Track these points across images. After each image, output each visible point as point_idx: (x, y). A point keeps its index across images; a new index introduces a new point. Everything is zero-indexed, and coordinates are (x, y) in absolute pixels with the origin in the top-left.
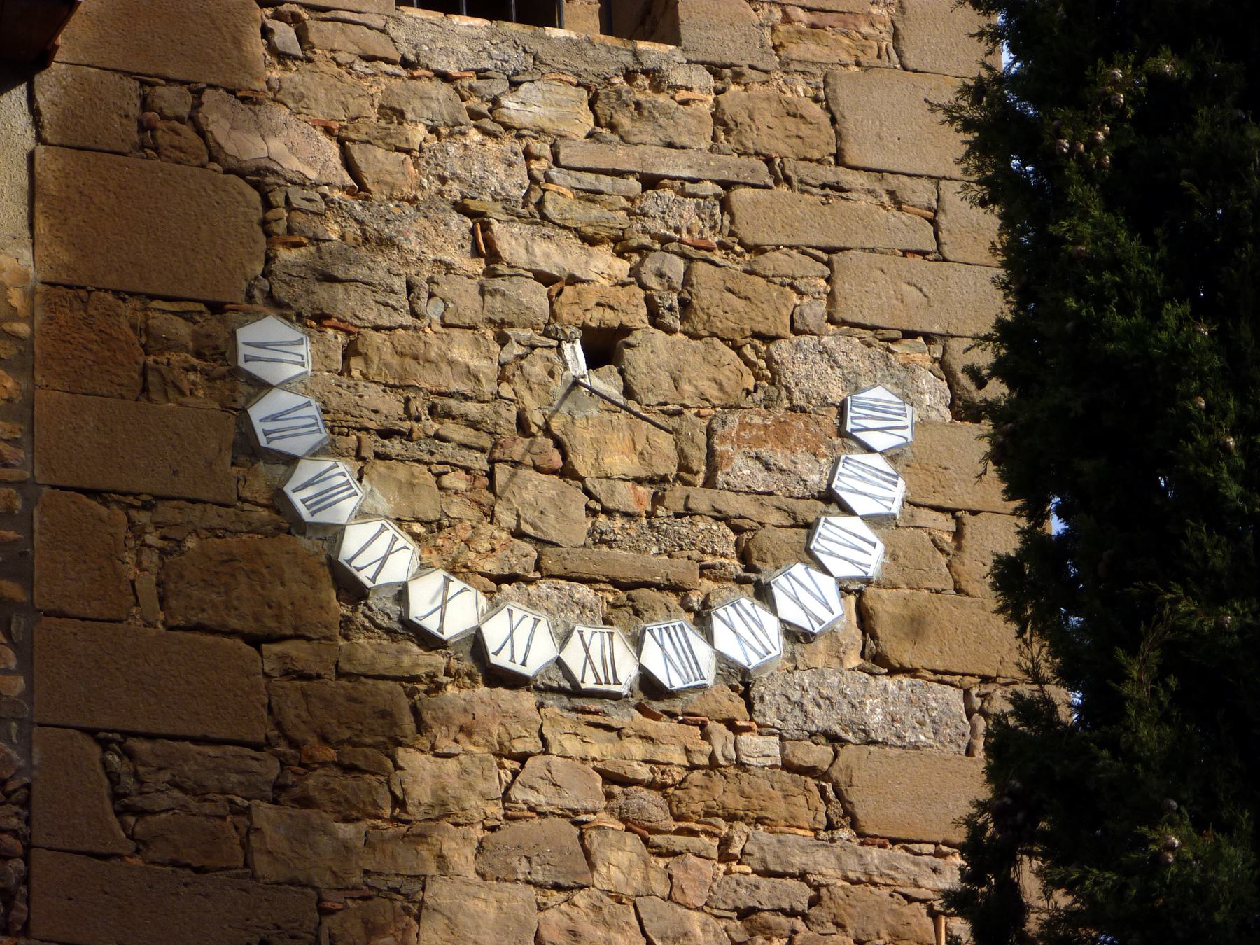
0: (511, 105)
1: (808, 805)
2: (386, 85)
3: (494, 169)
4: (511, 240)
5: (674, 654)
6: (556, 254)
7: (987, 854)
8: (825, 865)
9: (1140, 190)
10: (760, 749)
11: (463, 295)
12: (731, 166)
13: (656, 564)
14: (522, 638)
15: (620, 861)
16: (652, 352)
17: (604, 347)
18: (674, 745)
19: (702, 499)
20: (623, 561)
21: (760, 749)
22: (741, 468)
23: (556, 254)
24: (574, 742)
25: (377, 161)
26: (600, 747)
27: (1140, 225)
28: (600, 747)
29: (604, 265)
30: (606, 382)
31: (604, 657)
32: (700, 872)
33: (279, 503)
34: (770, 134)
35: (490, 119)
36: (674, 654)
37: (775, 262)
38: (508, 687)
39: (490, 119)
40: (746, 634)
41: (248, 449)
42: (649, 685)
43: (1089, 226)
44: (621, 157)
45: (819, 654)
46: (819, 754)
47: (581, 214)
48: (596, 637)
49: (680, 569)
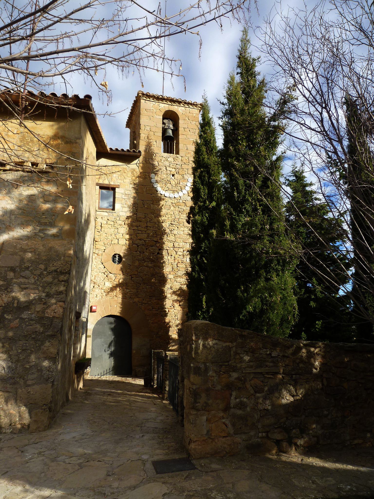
0: (168, 160)
1: (184, 205)
2: (160, 158)
3: (167, 164)
4: (168, 168)
5: (176, 195)
6: (171, 169)
7: (189, 214)
8: (184, 209)
9: (200, 177)
10: (181, 201)
11: (165, 172)
12: (182, 163)
13: (176, 189)
14: (167, 194)
15: (172, 208)
16: (176, 176)
17: (173, 175)
18: (176, 201)
19: (179, 185)
20: (174, 189)
21: (181, 201)
22: (181, 183)
23: (171, 169)
24: (170, 201)
25: (160, 163)
26: (171, 201)
27: (200, 180)
28: (171, 201)
29: (174, 170)
30: (173, 178)
31: (172, 195)
32: (177, 209)
33: (153, 186)
34: (184, 161)
35: (167, 160)
36: (176, 195)
37: (184, 170)
38: (157, 213)
39: (167, 160)
40: (181, 194)
41: (151, 182)
42: (175, 197)
43: (197, 179)
44: (175, 163)
45: (185, 195)
46: (184, 202)
47: (172, 167)
48: (171, 194)
49: (177, 190)
